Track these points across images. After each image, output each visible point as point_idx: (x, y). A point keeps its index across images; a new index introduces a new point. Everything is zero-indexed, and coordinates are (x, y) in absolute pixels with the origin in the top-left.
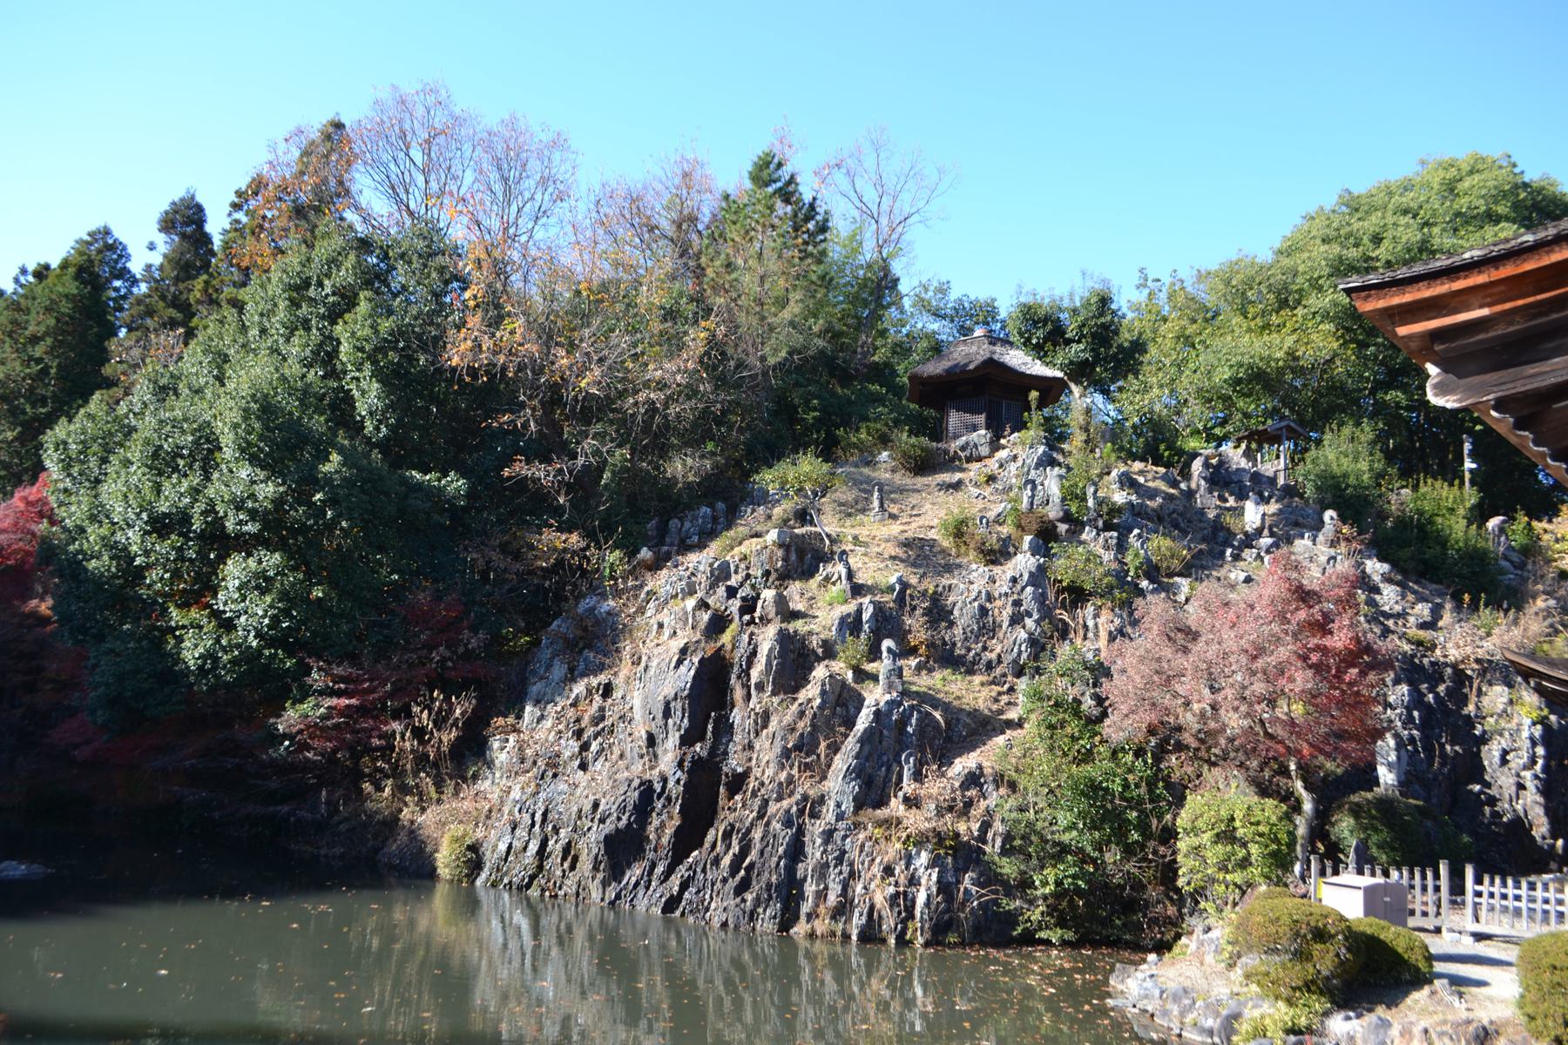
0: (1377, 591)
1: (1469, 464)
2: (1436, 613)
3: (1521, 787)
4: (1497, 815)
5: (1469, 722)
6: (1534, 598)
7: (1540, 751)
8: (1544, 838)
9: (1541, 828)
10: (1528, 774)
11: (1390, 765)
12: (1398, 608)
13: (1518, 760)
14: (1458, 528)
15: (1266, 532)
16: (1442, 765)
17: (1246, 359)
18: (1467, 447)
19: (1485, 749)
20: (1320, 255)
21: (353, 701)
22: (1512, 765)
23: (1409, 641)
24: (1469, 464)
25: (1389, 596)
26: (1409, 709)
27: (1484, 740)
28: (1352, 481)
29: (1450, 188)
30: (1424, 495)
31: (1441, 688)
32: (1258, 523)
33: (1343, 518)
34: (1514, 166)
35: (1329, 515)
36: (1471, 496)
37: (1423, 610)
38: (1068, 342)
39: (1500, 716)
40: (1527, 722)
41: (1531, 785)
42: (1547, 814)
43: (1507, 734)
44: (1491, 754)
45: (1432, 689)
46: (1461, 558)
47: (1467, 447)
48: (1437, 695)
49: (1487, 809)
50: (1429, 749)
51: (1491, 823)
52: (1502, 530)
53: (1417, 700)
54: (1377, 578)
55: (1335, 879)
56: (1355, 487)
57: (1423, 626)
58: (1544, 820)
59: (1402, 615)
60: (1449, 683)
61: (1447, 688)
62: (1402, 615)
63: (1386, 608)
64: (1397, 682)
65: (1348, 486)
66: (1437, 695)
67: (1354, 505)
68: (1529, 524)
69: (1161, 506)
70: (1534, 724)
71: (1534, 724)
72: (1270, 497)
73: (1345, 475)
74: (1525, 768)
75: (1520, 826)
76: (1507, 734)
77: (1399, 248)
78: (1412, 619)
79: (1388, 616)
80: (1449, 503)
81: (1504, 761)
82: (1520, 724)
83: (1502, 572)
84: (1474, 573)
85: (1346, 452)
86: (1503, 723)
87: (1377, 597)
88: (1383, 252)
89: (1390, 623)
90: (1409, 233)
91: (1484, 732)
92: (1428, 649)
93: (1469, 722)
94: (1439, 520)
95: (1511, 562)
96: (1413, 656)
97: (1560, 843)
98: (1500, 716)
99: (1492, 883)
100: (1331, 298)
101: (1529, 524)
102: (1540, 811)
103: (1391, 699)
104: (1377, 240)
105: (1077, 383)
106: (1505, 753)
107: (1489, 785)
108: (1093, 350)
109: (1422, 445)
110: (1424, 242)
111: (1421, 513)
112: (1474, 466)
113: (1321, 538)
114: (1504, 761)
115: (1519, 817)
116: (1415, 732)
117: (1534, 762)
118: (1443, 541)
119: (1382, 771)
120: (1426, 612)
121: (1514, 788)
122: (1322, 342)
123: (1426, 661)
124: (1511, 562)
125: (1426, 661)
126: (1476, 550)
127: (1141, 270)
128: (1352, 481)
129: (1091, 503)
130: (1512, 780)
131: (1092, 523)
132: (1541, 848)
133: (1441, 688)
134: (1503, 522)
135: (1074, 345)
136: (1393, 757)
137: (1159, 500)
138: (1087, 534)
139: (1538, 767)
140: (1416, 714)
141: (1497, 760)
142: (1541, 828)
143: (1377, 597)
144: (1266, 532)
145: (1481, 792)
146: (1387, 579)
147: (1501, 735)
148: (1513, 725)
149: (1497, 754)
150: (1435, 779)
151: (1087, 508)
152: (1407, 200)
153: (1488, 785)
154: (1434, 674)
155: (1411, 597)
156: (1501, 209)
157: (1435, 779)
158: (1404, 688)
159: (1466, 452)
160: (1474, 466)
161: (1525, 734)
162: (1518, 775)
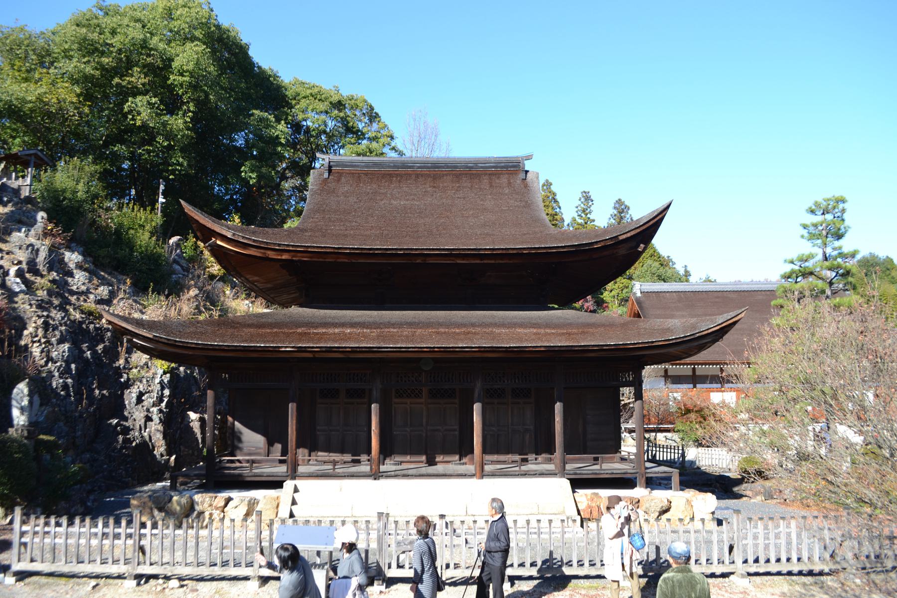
0: (71, 275)
1: (161, 200)
2: (113, 294)
3: (148, 419)
4: (127, 441)
5: (118, 372)
6: (189, 290)
7: (167, 392)
8: (162, 455)
9: (160, 448)
10: (155, 410)
11: (22, 409)
12: (84, 288)
13: (148, 400)
14: (144, 239)
16: (90, 404)
18: (162, 187)
19: (127, 392)
22: (145, 403)
23: (82, 312)
24: (161, 200)
25: (79, 280)
26: (68, 362)
27: (128, 385)
28: (68, 195)
29: (169, 14)
30: (125, 214)
31: (100, 347)
33: (50, 219)
34: (212, 11)
35: (41, 215)
36: (158, 218)
37: (103, 291)
39: (142, 367)
40: (160, 372)
41: (156, 418)
42: (164, 438)
43: (144, 381)
44: (130, 396)
45: (92, 348)
46: (142, 258)
47: (162, 187)
48: (94, 353)
49: (121, 437)
50: (78, 393)
51: (122, 448)
52: (178, 245)
53: (76, 355)
54: (72, 266)
55: (432, 469)
56: (70, 200)
57: (100, 302)
58: (163, 442)
59: (87, 293)
60: (107, 344)
61: (104, 347)
62: (87, 293)
63: (74, 288)
64: (61, 341)
65: (65, 198)
66: (94, 353)
67: (67, 216)
68: (196, 243)
70: (165, 373)
71: (165, 373)
73: (64, 191)
74: (154, 405)
75: (146, 447)
76: (144, 381)
77: (127, 40)
78: (92, 297)
79: (72, 293)
80: (141, 223)
81: (139, 400)
82: (155, 374)
83: (174, 272)
84: (150, 270)
85: (72, 177)
86: (143, 373)
87: (70, 279)
88: (116, 41)
89: (73, 299)
90: (136, 33)
91: (128, 379)
92: (96, 318)
93: (118, 372)
94: (132, 232)
95: (182, 267)
96: (81, 323)
97: (173, 458)
98: (142, 367)
101: (196, 243)
102: (160, 436)
103: (54, 354)
104: (114, 32)
106: (140, 395)
107: (126, 419)
109: (136, 183)
110: (145, 41)
111: (121, 225)
112: (164, 200)
113: (32, 232)
114: (139, 400)
115: (145, 442)
116: (69, 380)
117: (161, 401)
118: (130, 245)
119: (16, 412)
120: (106, 292)
121: (143, 421)
122: (67, 94)
123: (91, 326)
124: (182, 267)
125: (91, 326)
126: (153, 254)
130: (143, 414)
132: (160, 462)
133: (100, 347)
134: (179, 240)
136: (25, 402)
139: (163, 405)
140: (73, 366)
141: (134, 400)
142: (160, 448)
143: (70, 279)
145: (118, 424)
146: (79, 266)
147: (141, 382)
148: (150, 374)
149: (134, 395)
150: (81, 416)
152: (138, 14)
153: (126, 419)
154: (98, 336)
155: (95, 281)
156: (198, 33)
157: (81, 416)
158: (66, 346)
159: (161, 191)
160: (164, 200)
161: (157, 380)
162: (148, 410)
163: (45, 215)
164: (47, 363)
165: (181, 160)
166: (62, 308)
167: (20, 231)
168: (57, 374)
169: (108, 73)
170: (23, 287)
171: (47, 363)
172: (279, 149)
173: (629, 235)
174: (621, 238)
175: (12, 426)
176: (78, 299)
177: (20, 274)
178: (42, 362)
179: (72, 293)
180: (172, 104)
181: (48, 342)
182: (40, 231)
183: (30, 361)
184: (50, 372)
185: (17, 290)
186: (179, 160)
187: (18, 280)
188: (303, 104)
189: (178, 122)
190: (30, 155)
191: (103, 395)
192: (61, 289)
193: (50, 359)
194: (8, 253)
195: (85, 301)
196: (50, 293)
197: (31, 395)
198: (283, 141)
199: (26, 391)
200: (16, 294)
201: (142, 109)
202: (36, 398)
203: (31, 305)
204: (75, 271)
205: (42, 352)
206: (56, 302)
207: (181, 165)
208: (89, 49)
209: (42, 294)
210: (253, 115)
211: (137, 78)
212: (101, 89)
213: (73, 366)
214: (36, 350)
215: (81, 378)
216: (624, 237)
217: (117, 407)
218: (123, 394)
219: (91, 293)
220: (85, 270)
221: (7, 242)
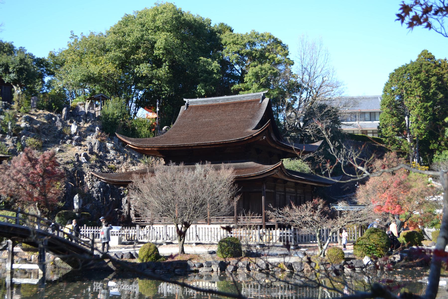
0: (109, 152)
11: (77, 203)
12: (113, 158)
15: (78, 134)
17: (86, 74)
20: (111, 38)
21: (292, 202)
23: (109, 168)
27: (124, 196)
32: (75, 131)
38: (10, 73)
50: (103, 199)
54: (109, 148)
65: (109, 118)
69: (39, 127)
72: (89, 121)
78: (115, 161)
79: (107, 160)
88: (130, 39)
89: (107, 163)
91: (124, 194)
99: (89, 229)
100: (116, 53)
105: (16, 86)
108: (18, 76)
119: (75, 204)
122: (111, 68)
127: (71, 32)
128: (110, 116)
129: (9, 127)
131: (9, 134)
134: (167, 128)
135: (12, 74)
137: (39, 125)
138: (8, 137)
140: (102, 189)
141: (125, 202)
143: (108, 154)
144: (78, 134)
151: (9, 129)
163: (98, 128)
164: (92, 188)
165: (167, 88)
166: (100, 167)
167: (90, 135)
168: (95, 192)
169: (127, 54)
170: (86, 160)
171: (92, 188)
172: (214, 75)
173: (256, 134)
174: (254, 135)
175: (74, 209)
176: (109, 162)
177: (85, 155)
178: (90, 188)
179: (107, 160)
180: (158, 63)
181: (93, 181)
182: (97, 135)
183: (85, 188)
184: (93, 192)
185: (84, 162)
186: (166, 88)
187: (84, 158)
188: (228, 47)
189: (163, 71)
190: (100, 96)
191: (113, 200)
192: (102, 160)
193: (93, 187)
194: (84, 146)
195: (112, 163)
196: (96, 161)
197: (79, 198)
198: (215, 71)
199: (78, 197)
200: (83, 163)
201: (144, 69)
202: (81, 200)
203: (87, 167)
204: (110, 151)
205: (90, 184)
206: (98, 165)
207: (166, 90)
208: (119, 45)
209: (93, 162)
210: (201, 59)
211: (141, 55)
212: (124, 64)
213: (102, 189)
214: (88, 184)
215: (104, 194)
216: (255, 135)
217: (119, 205)
218: (122, 199)
219: (116, 159)
220: (114, 150)
221: (85, 140)
